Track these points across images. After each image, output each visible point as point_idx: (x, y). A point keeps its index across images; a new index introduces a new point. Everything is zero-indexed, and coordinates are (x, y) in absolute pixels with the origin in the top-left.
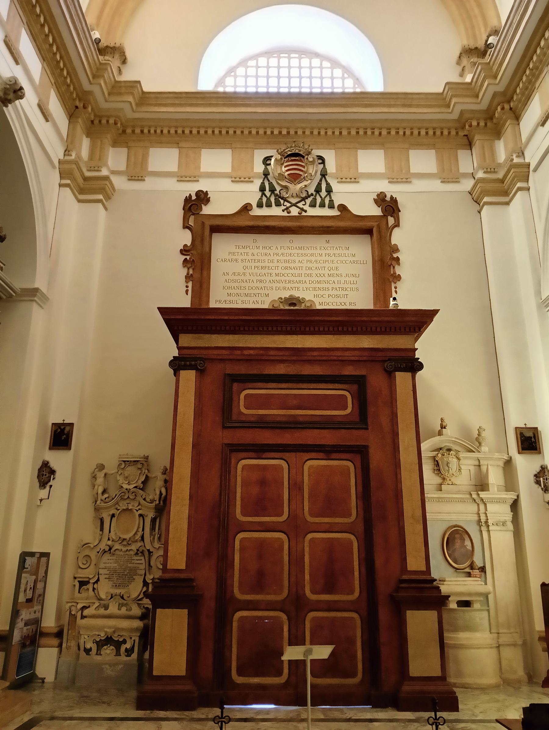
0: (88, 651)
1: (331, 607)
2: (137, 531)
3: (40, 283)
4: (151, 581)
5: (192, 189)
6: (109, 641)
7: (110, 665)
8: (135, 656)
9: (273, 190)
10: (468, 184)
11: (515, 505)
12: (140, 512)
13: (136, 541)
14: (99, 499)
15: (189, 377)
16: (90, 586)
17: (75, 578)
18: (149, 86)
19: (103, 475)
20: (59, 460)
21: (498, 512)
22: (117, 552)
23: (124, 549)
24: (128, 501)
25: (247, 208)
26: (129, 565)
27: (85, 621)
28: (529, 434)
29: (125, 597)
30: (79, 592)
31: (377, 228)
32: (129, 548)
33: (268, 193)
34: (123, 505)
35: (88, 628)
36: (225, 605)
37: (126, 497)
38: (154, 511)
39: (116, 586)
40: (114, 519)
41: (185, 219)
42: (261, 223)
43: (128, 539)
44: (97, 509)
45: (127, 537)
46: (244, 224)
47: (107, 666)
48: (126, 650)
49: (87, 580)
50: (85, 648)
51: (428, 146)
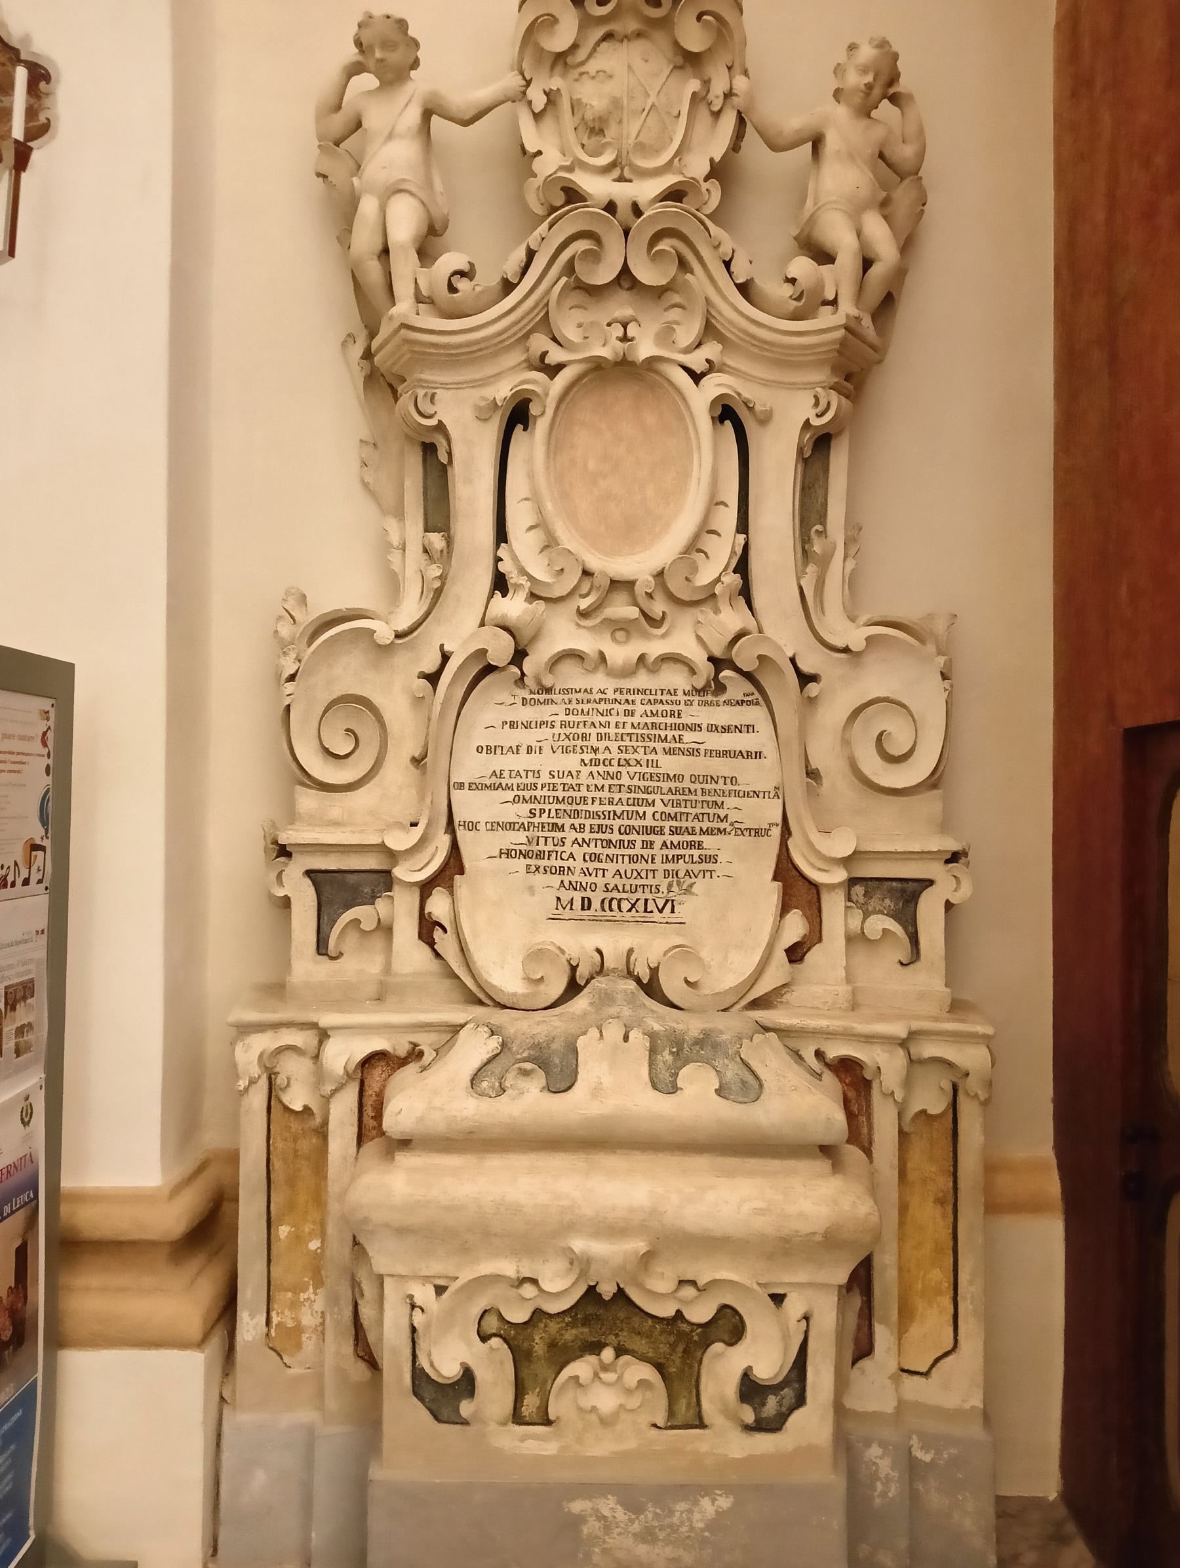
0: (445, 1397)
2: (706, 529)
4: (839, 875)
6: (603, 1317)
7: (632, 1498)
8: (811, 1425)
12: (714, 386)
13: (709, 597)
14: (404, 290)
16: (401, 909)
17: (284, 852)
19: (413, 115)
22: (572, 677)
23: (620, 653)
24: (621, 306)
26: (670, 764)
27: (389, 1188)
29: (671, 985)
30: (321, 947)
32: (655, 648)
34: (587, 335)
35: (428, 1232)
37: (605, 274)
38: (822, 376)
39: (586, 904)
40: (529, 448)
43: (645, 581)
44: (382, 382)
45: (638, 565)
47: (608, 1506)
48: (751, 1390)
49: (372, 862)
50: (418, 1374)
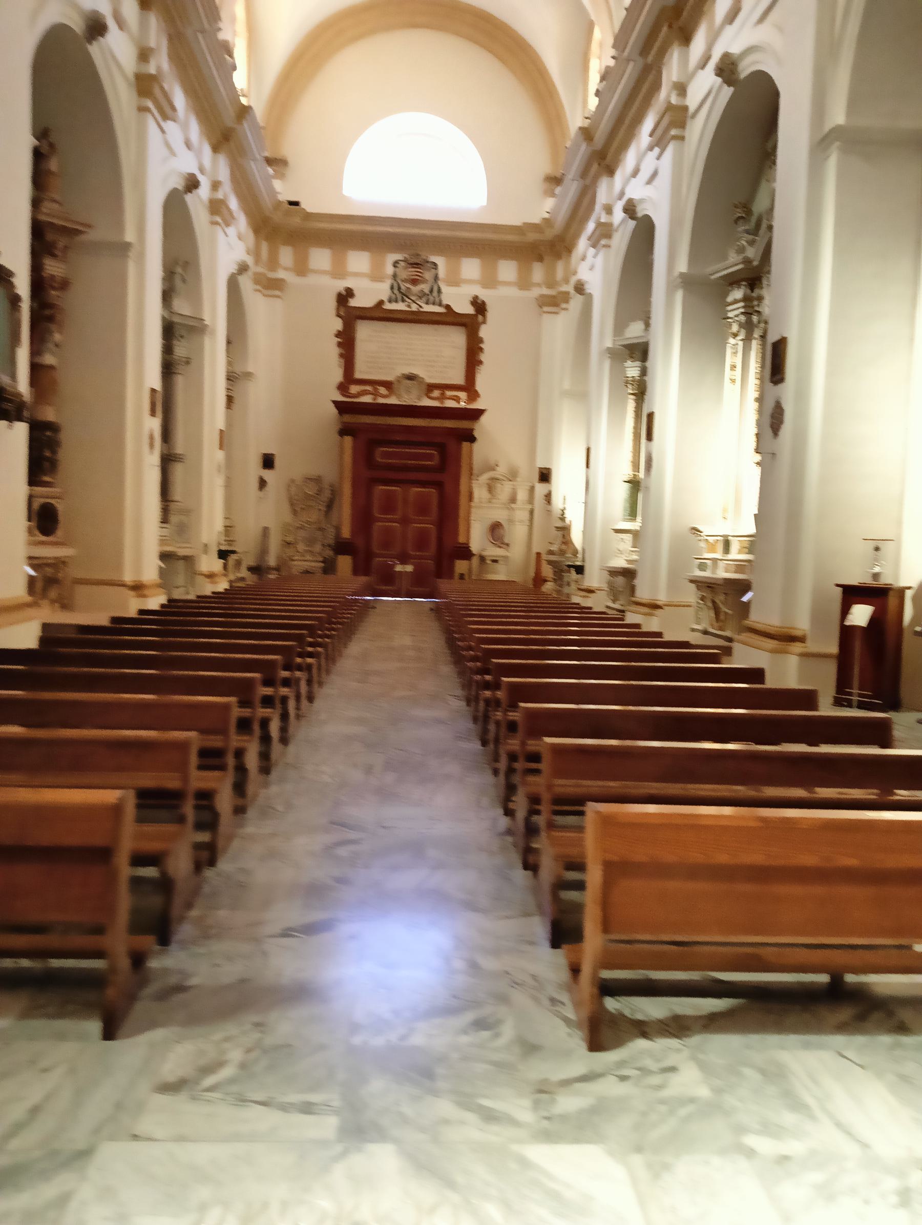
1: (420, 558)
3: (250, 369)
5: (341, 285)
9: (399, 288)
10: (536, 292)
11: (532, 512)
15: (348, 440)
18: (309, 210)
20: (268, 475)
21: (521, 515)
25: (381, 303)
28: (545, 472)
31: (471, 323)
33: (396, 291)
36: (369, 556)
41: (338, 309)
42: (392, 316)
46: (378, 314)
51: (512, 259)
